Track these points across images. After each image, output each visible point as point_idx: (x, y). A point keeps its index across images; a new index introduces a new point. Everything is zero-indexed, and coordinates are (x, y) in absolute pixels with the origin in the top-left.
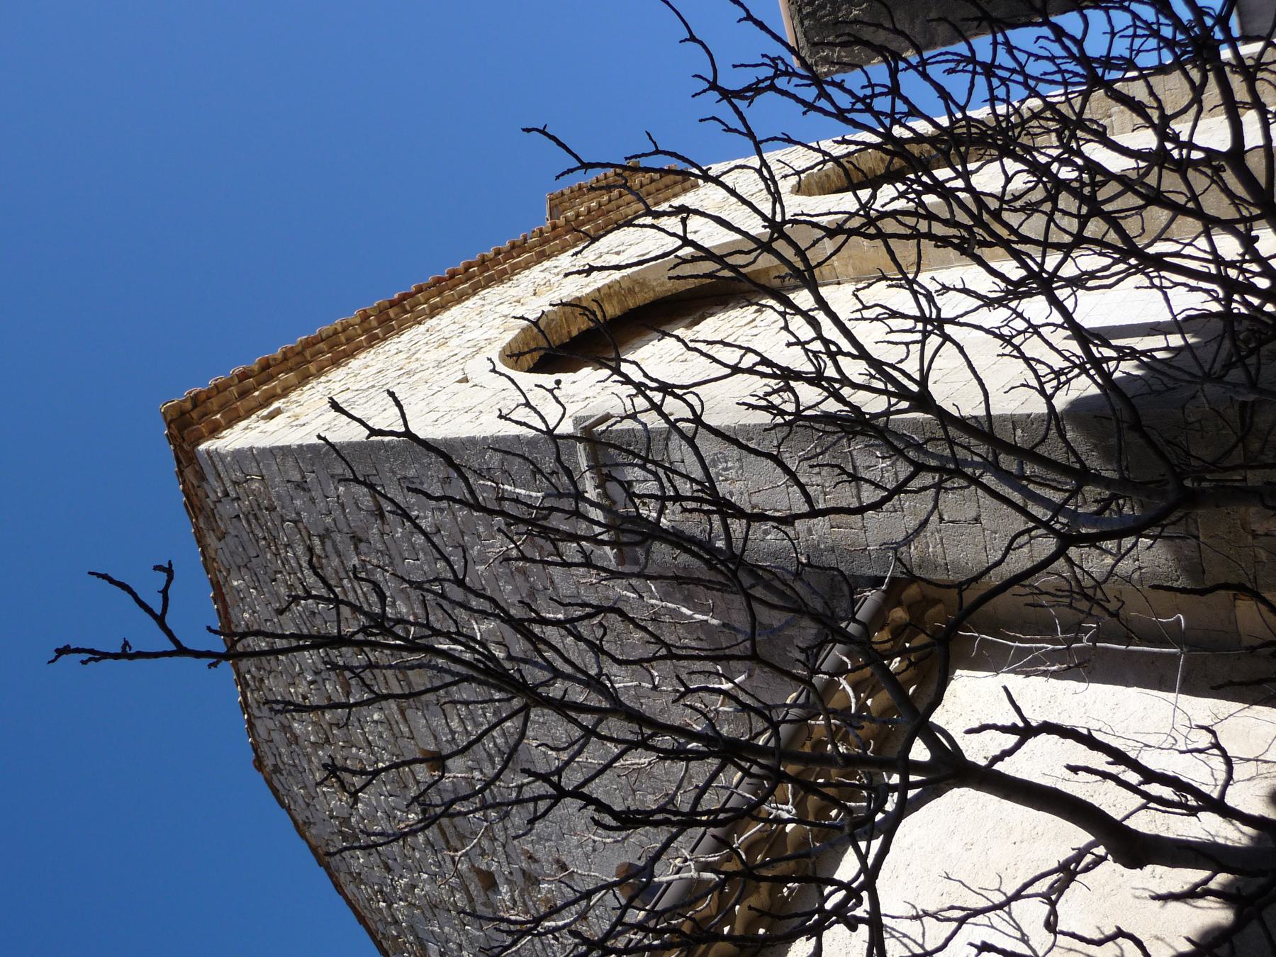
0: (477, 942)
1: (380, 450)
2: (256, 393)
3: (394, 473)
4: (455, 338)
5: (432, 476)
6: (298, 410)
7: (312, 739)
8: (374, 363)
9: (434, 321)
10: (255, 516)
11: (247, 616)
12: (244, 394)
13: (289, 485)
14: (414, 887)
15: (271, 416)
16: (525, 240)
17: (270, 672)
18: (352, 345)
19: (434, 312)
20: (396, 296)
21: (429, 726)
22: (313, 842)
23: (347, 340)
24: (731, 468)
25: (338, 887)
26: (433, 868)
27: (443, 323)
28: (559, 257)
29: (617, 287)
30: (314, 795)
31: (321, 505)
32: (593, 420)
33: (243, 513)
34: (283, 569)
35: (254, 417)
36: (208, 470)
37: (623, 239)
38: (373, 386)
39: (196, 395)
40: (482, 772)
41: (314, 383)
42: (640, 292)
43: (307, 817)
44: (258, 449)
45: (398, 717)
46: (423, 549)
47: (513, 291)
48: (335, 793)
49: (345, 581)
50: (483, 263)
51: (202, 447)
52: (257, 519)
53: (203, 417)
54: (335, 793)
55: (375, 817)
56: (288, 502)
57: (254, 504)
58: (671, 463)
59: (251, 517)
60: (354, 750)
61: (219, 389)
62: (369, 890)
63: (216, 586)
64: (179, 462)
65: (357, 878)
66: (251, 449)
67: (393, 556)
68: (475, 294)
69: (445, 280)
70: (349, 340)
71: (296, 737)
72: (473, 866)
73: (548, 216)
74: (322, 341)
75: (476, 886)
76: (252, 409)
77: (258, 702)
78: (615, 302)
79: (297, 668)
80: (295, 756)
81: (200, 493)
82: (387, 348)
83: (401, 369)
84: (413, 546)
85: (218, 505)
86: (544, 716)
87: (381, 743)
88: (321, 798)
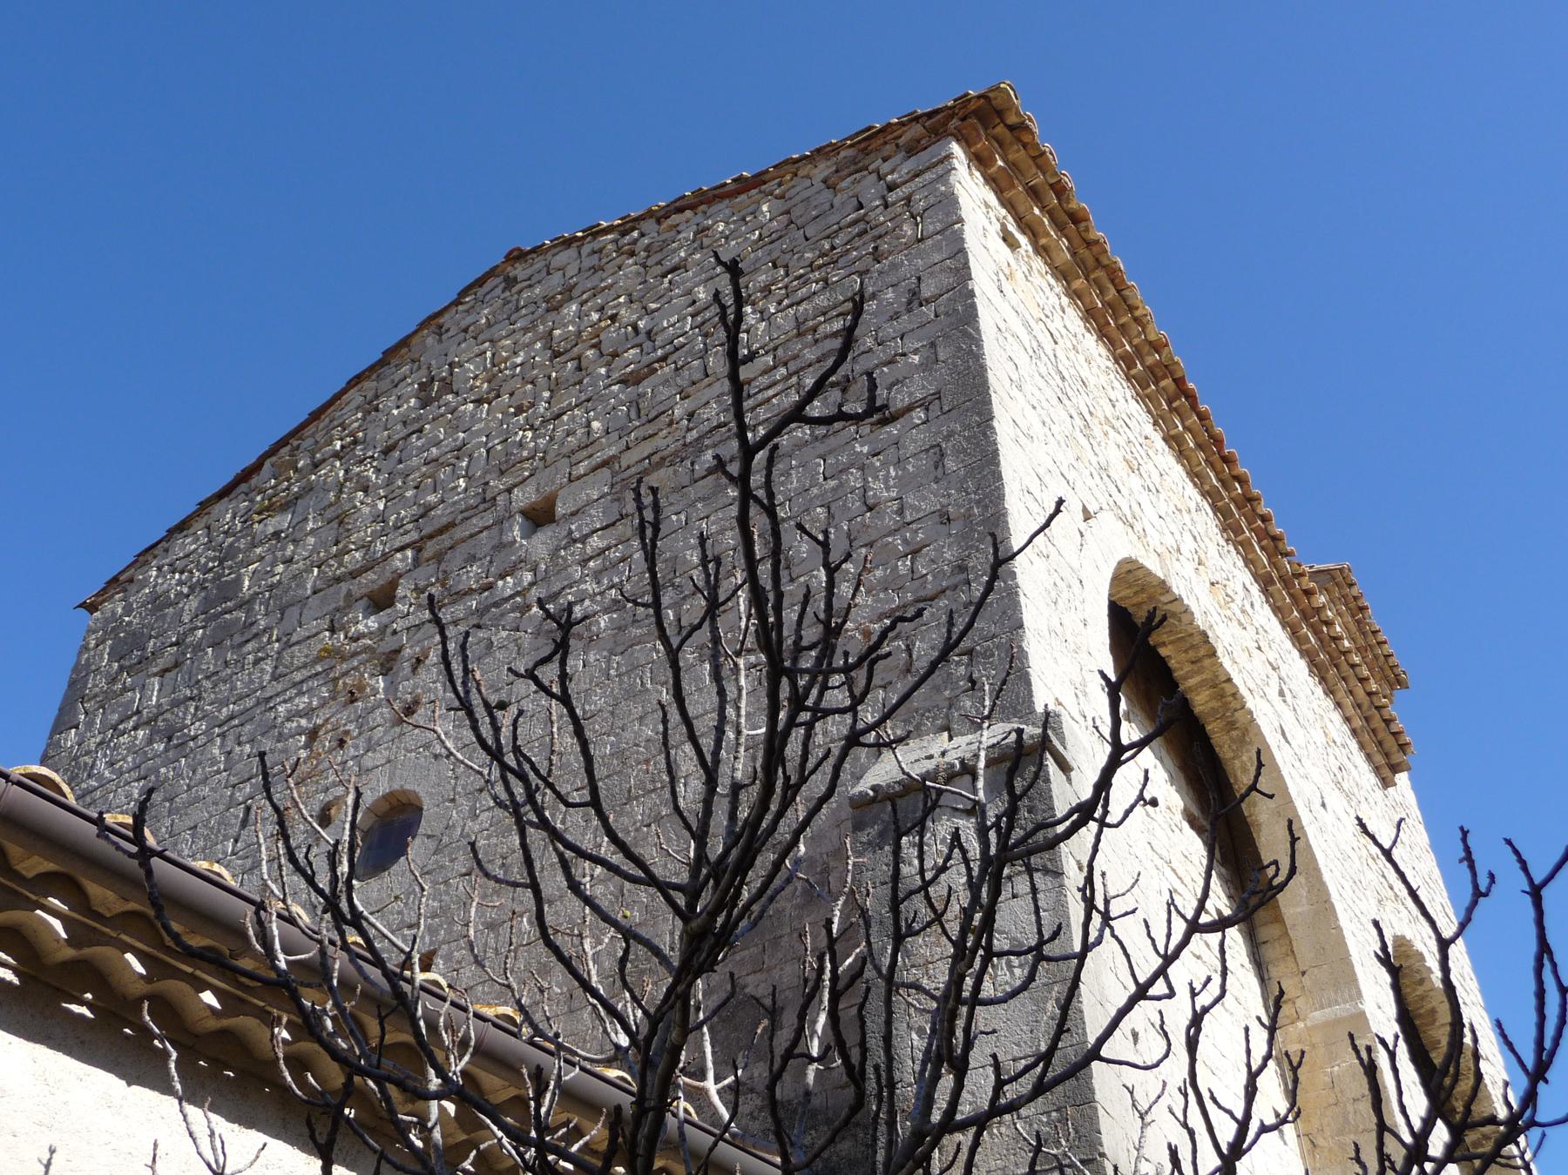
0: (297, 585)
1: (980, 414)
2: (1037, 211)
3: (947, 438)
4: (1141, 482)
5: (949, 495)
6: (1019, 275)
7: (557, 332)
8: (1095, 370)
9: (1160, 444)
10: (864, 232)
11: (721, 229)
12: (1034, 193)
13: (914, 280)
14: (366, 490)
15: (1007, 239)
16: (1286, 554)
17: (644, 266)
18: (1115, 334)
19: (1172, 440)
20: (1191, 385)
21: (590, 503)
22: (415, 340)
23: (1122, 325)
24: (1012, 973)
25: (357, 380)
26: (393, 518)
27: (1159, 460)
28: (1266, 606)
29: (1234, 705)
30: (481, 338)
31: (890, 330)
32: (1060, 748)
33: (866, 214)
34: (791, 278)
35: (1004, 212)
36: (923, 158)
37: (1301, 695)
38: (1063, 378)
39: (1027, 127)
40: (532, 584)
41: (1059, 289)
42: (1231, 739)
43: (448, 331)
44: (961, 231)
45: (599, 457)
46: (841, 485)
47: (1213, 550)
48: (485, 368)
49: (783, 371)
50: (1250, 500)
51: (956, 148)
52: (860, 235)
53: (998, 141)
54: (485, 368)
55: (457, 429)
56: (892, 279)
57: (882, 230)
58: (1009, 878)
59: (862, 226)
60: (546, 394)
61: (1039, 158)
62: (356, 425)
63: (758, 180)
64: (930, 115)
65: (371, 407)
66: (961, 220)
67: (827, 441)
68: (1204, 494)
69: (1220, 449)
70: (1122, 328)
71: (557, 309)
72: (400, 576)
73: (1317, 567)
74: (1118, 291)
75: (373, 582)
76: (1013, 207)
77: (600, 251)
78: (1214, 704)
79: (653, 306)
80: (532, 308)
81: (889, 148)
82: (1116, 384)
83: (1091, 413)
84: (844, 470)
85: (874, 176)
86: (619, 675)
87: (559, 434)
88: (476, 350)
